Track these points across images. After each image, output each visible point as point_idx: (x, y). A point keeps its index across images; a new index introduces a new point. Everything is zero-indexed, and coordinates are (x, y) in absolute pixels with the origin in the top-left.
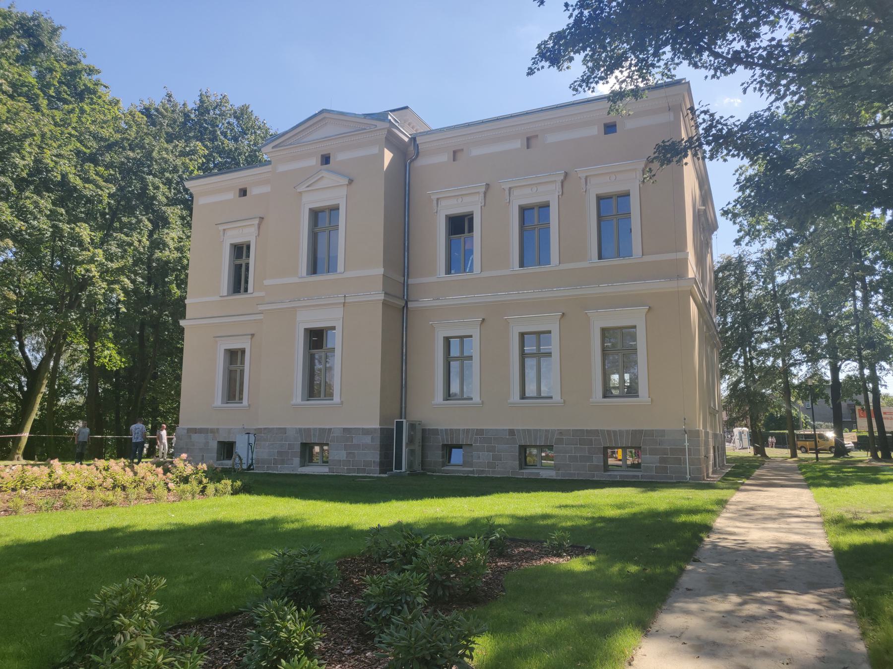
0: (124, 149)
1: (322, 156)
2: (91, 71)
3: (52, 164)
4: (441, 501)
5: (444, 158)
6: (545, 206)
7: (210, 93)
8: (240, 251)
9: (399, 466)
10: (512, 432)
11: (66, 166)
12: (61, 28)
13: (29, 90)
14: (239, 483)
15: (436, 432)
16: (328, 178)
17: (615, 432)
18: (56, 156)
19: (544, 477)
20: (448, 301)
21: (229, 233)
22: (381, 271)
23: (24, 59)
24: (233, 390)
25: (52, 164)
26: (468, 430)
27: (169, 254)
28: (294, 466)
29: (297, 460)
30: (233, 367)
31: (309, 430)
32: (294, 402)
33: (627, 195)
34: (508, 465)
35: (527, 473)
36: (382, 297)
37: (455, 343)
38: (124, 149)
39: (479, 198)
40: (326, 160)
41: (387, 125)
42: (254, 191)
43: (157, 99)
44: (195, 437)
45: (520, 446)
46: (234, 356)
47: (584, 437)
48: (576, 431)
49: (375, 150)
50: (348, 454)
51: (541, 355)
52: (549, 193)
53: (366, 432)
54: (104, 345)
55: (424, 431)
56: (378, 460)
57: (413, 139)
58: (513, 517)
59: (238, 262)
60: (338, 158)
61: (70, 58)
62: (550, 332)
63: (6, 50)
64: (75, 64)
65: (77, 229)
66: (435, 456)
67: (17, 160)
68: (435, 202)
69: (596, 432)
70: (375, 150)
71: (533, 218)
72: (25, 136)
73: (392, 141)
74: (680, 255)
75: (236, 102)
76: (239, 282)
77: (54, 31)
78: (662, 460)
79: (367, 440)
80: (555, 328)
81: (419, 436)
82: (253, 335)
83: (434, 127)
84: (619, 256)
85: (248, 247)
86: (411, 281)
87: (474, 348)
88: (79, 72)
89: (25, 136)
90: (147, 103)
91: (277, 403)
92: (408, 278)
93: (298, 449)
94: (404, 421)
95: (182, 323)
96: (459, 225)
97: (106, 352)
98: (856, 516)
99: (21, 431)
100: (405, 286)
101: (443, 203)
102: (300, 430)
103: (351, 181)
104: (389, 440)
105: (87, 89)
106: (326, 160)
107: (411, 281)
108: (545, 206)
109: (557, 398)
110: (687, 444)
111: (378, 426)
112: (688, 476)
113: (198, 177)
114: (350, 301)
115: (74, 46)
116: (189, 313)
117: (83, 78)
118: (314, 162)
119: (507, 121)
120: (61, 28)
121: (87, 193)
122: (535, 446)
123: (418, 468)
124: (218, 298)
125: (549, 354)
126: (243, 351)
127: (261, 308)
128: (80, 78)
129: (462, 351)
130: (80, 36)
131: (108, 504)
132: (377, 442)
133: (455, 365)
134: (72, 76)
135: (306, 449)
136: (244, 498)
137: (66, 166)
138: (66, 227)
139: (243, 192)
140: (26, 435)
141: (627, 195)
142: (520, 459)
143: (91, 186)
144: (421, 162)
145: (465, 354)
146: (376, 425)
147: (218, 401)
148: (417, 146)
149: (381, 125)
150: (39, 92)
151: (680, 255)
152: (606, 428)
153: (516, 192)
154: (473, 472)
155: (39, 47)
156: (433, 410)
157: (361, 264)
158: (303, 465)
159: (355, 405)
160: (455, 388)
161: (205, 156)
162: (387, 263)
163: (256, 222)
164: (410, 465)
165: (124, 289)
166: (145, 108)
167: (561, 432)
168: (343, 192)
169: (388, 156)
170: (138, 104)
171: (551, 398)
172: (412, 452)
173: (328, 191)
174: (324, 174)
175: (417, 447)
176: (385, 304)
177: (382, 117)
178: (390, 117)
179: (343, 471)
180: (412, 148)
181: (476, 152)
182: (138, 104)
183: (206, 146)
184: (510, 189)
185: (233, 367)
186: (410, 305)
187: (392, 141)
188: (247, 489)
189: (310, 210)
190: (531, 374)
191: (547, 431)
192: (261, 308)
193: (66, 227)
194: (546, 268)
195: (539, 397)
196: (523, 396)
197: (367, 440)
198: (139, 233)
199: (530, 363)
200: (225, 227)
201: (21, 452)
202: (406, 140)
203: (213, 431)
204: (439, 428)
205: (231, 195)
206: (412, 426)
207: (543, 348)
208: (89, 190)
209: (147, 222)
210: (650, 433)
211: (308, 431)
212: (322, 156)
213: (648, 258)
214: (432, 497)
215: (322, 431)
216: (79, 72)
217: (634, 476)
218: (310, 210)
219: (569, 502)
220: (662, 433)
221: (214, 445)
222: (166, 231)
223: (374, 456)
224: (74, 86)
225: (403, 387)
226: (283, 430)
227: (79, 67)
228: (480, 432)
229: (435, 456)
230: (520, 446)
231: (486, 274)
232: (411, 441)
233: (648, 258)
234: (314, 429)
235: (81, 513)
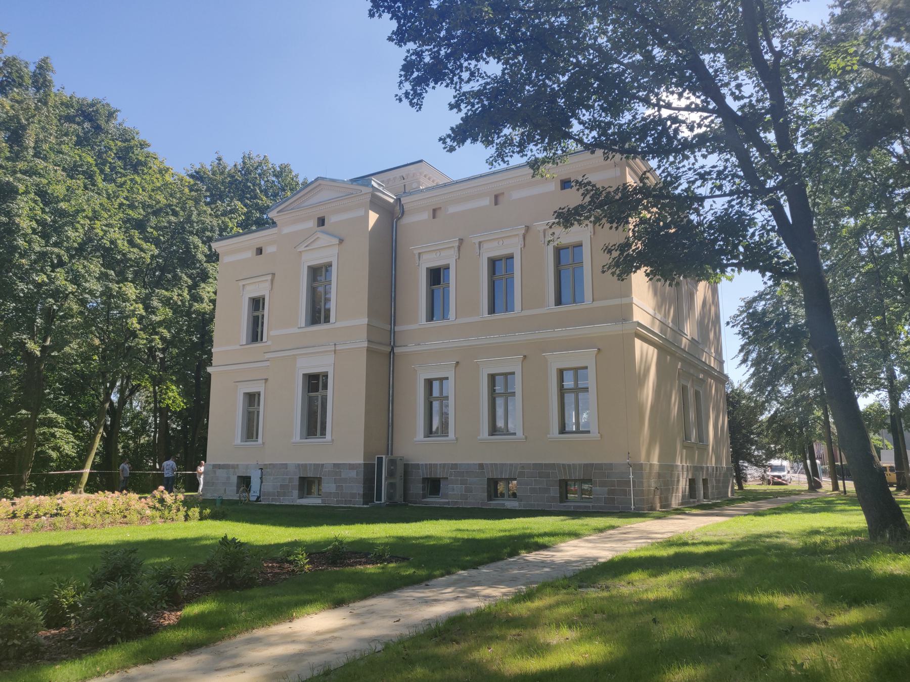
0: (167, 214)
1: (319, 219)
2: (143, 145)
3: (101, 233)
4: (347, 527)
5: (426, 216)
6: (510, 257)
7: (253, 155)
8: (257, 303)
9: (379, 498)
10: (481, 466)
11: (116, 234)
12: (117, 111)
13: (88, 168)
14: (208, 511)
15: (417, 466)
16: (324, 240)
17: (569, 465)
18: (106, 226)
19: (509, 507)
20: (429, 347)
21: (248, 288)
22: (365, 321)
23: (81, 142)
24: (251, 431)
25: (101, 233)
26: (444, 465)
27: (206, 306)
28: (294, 499)
29: (296, 493)
30: (251, 409)
31: (306, 465)
32: (294, 440)
33: (580, 245)
34: (479, 496)
35: (495, 504)
36: (365, 344)
37: (436, 385)
38: (167, 214)
39: (453, 253)
40: (321, 222)
41: (370, 190)
42: (269, 250)
43: (207, 162)
44: (220, 472)
45: (490, 480)
46: (252, 399)
47: (542, 470)
48: (536, 466)
49: (361, 213)
50: (338, 487)
51: (578, 390)
52: (513, 246)
53: (352, 467)
54: (168, 388)
55: (406, 466)
56: (362, 492)
57: (398, 200)
58: (393, 537)
59: (256, 314)
60: (331, 220)
61: (125, 136)
62: (586, 368)
63: (65, 138)
64: (129, 141)
65: (124, 289)
66: (417, 489)
67: (70, 233)
68: (417, 256)
69: (553, 466)
70: (361, 213)
71: (499, 268)
72: (77, 212)
73: (377, 203)
74: (625, 301)
75: (276, 161)
76: (256, 335)
77: (111, 115)
78: (610, 492)
79: (353, 474)
80: (518, 370)
81: (400, 470)
82: (266, 380)
83: (455, 178)
84: (575, 302)
85: (264, 299)
86: (397, 329)
87: (450, 388)
88: (132, 148)
89: (77, 212)
90: (197, 167)
91: (283, 444)
92: (395, 325)
93: (296, 483)
94: (384, 457)
95: (209, 369)
96: (436, 276)
97: (170, 394)
98: (680, 538)
99: (83, 467)
100: (392, 333)
101: (424, 257)
102: (299, 465)
103: (341, 241)
104: (370, 473)
105: (139, 163)
106: (321, 222)
107: (397, 329)
108: (510, 257)
109: (520, 434)
110: (631, 477)
111: (362, 462)
112: (633, 507)
113: (238, 235)
114: (340, 350)
115: (128, 125)
116: (215, 361)
117: (136, 152)
118: (312, 224)
119: (476, 181)
120: (117, 111)
121: (132, 257)
122: (575, 481)
123: (399, 498)
124: (238, 347)
125: (586, 390)
126: (259, 394)
127: (268, 356)
128: (133, 153)
129: (576, 381)
130: (138, 113)
131: (86, 526)
132: (361, 476)
133: (500, 402)
134: (124, 154)
135: (245, 482)
136: (209, 523)
137: (116, 234)
138: (115, 287)
139: (260, 251)
140: (87, 471)
141: (580, 245)
142: (488, 491)
143: (135, 250)
144: (407, 220)
145: (509, 391)
146: (361, 461)
147: (238, 441)
148: (402, 206)
149: (365, 190)
150: (95, 169)
151: (625, 301)
152: (571, 462)
153: (485, 246)
154: (448, 503)
155: (98, 129)
156: (417, 447)
157: (351, 316)
158: (301, 497)
159: (345, 444)
160: (500, 423)
161: (244, 214)
162: (372, 313)
163: (269, 277)
164: (390, 497)
165: (163, 339)
166: (197, 172)
167: (523, 466)
168: (335, 250)
169: (373, 217)
170: (189, 168)
171: (588, 432)
172: (391, 486)
173: (322, 251)
174: (319, 235)
175: (398, 481)
176: (369, 351)
177: (364, 180)
178: (373, 183)
179: (333, 502)
180: (398, 208)
181: (452, 210)
182: (189, 168)
183: (246, 205)
184: (480, 243)
185: (251, 409)
186: (396, 350)
187: (377, 203)
188: (215, 516)
189: (309, 267)
190: (500, 412)
191: (511, 465)
192: (268, 356)
193: (115, 287)
194: (509, 315)
195: (578, 432)
196: (563, 430)
197: (353, 474)
198: (180, 288)
199: (569, 398)
200: (244, 282)
201: (82, 486)
202: (392, 201)
203: (234, 467)
204: (421, 463)
205: (250, 254)
206: (392, 462)
207: (581, 384)
208: (134, 253)
209: (185, 278)
210: (599, 466)
211: (305, 466)
212: (319, 219)
213: (597, 304)
214: (362, 523)
215: (317, 466)
216: (132, 148)
217: (586, 507)
218: (309, 267)
219: (462, 527)
220: (610, 466)
221: (234, 479)
222: (203, 285)
223: (358, 489)
224: (130, 158)
225: (390, 426)
226: (285, 466)
227: (132, 144)
228: (455, 466)
229: (417, 489)
230: (490, 480)
231: (459, 321)
232: (391, 474)
233: (597, 304)
234: (310, 465)
235: (64, 532)
